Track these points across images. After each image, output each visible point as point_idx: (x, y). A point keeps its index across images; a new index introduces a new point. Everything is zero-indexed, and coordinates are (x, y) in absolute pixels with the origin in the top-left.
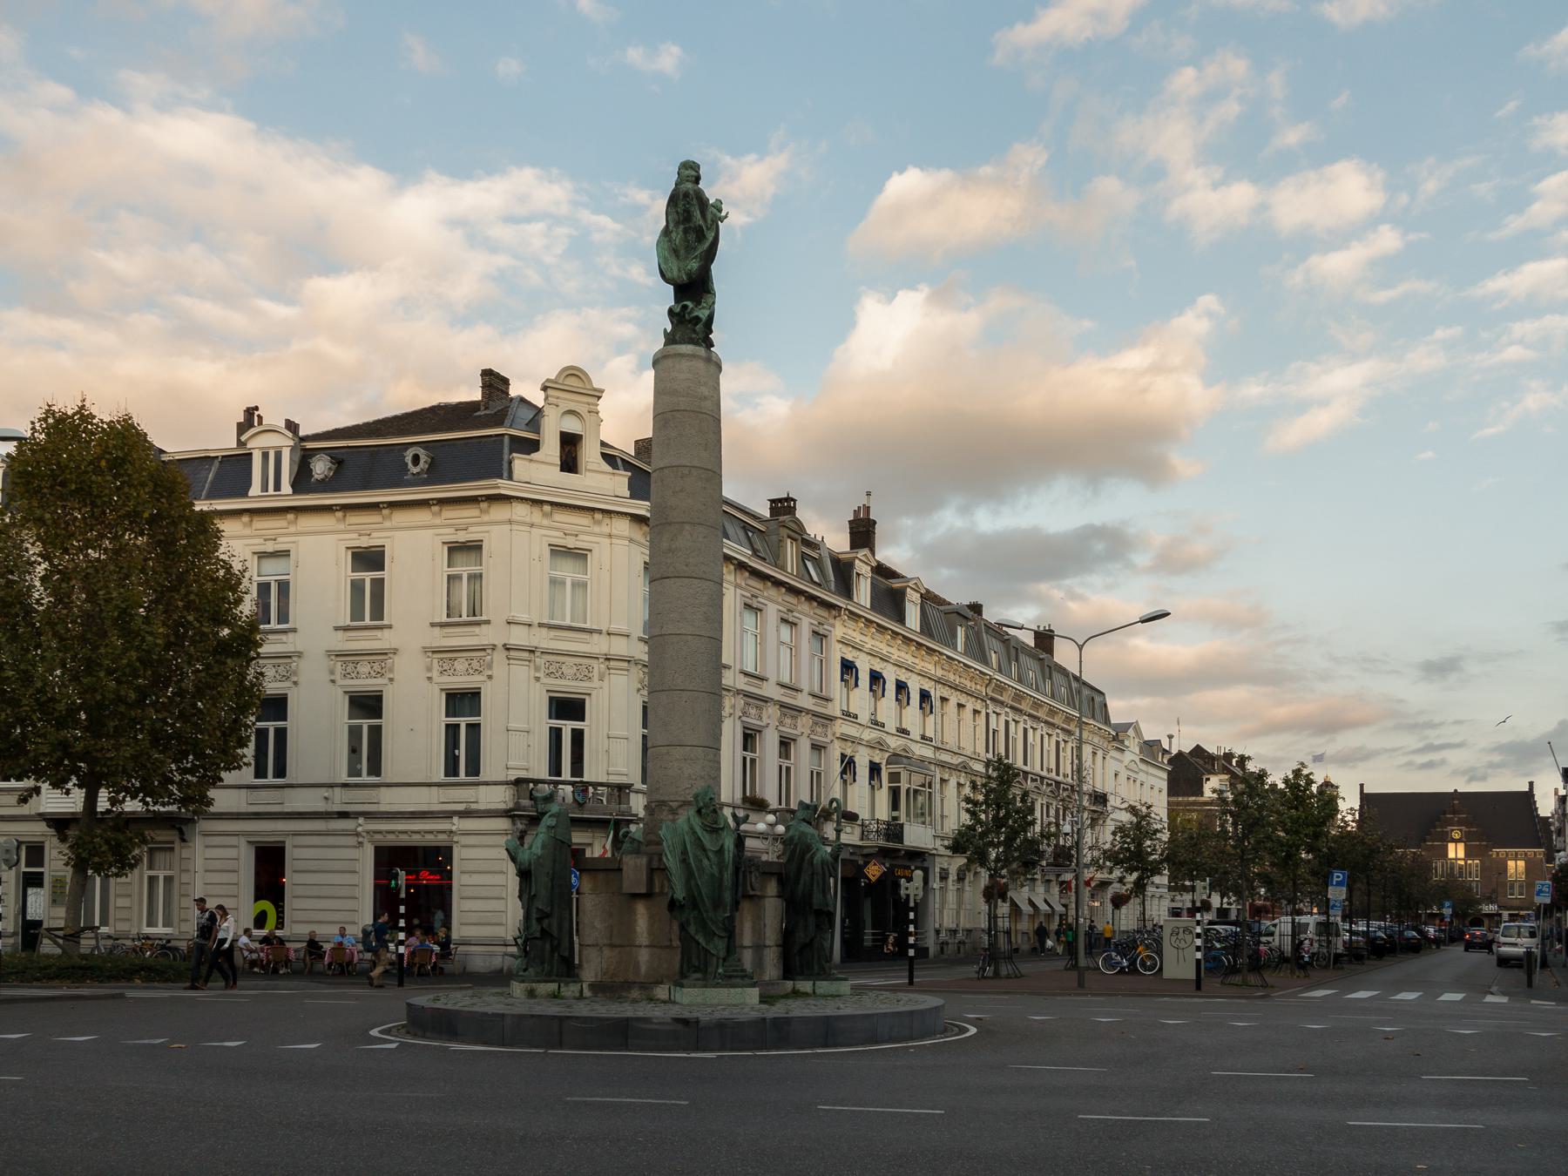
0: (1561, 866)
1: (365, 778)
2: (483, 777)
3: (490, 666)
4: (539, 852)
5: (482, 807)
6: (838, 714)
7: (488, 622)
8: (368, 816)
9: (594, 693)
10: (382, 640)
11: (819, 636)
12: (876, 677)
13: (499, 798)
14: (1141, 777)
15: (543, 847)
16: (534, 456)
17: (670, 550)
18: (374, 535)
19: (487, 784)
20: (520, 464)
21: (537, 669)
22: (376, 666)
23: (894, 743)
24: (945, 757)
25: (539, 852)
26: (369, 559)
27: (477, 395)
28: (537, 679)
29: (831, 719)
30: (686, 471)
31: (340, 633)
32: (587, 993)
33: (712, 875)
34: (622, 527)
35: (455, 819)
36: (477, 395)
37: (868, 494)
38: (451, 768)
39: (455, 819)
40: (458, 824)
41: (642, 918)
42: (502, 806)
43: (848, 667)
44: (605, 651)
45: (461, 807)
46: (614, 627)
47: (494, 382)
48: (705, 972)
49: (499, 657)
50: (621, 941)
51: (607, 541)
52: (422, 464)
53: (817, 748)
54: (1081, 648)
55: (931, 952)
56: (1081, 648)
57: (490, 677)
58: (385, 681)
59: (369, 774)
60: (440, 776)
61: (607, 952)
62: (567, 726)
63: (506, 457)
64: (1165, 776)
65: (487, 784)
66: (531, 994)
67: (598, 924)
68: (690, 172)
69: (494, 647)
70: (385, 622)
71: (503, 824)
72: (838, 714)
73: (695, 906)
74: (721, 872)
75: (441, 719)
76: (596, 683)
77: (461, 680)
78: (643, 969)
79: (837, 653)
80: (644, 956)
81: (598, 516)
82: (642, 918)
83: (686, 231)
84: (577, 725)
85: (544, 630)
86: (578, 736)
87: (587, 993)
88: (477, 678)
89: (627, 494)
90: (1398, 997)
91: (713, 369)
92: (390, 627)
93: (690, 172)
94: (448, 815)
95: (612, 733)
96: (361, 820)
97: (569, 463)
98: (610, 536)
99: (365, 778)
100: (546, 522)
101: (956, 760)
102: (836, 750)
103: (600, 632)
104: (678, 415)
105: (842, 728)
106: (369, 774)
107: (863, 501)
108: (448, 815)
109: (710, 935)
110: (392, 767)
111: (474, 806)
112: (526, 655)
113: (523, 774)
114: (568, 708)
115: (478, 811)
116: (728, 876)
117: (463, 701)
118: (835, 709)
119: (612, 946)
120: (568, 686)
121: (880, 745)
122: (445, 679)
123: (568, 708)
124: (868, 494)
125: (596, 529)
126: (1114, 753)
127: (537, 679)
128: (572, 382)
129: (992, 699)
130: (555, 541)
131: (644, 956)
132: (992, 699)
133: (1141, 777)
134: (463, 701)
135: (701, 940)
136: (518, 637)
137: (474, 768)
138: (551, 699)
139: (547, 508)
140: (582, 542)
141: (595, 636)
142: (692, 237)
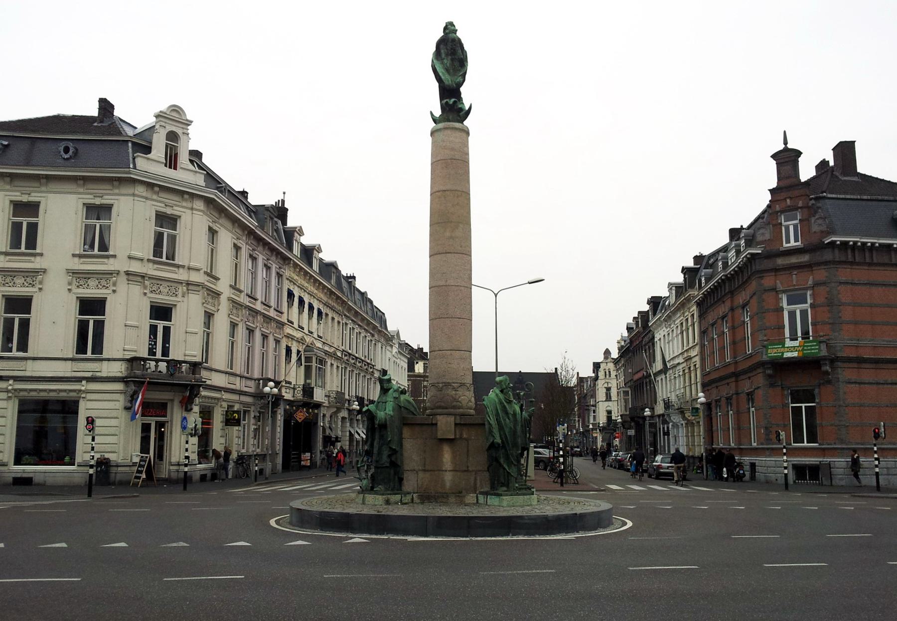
1: (15, 353)
2: (105, 355)
3: (114, 284)
5: (104, 374)
7: (114, 256)
8: (16, 379)
9: (179, 305)
10: (36, 263)
11: (279, 276)
12: (301, 301)
13: (118, 369)
14: (398, 361)
18: (33, 194)
20: (142, 163)
21: (145, 288)
22: (29, 280)
24: (327, 348)
26: (30, 209)
27: (94, 112)
29: (283, 324)
30: (459, 193)
31: (76, 259)
34: (199, 205)
35: (84, 382)
36: (94, 112)
38: (81, 347)
39: (84, 382)
40: (84, 386)
41: (447, 456)
42: (119, 375)
43: (291, 294)
44: (186, 279)
45: (89, 375)
46: (192, 264)
47: (106, 106)
48: (508, 486)
49: (123, 279)
50: (433, 468)
51: (189, 212)
52: (71, 152)
53: (277, 342)
58: (36, 289)
59: (18, 350)
60: (70, 352)
61: (421, 475)
63: (131, 155)
66: (388, 502)
67: (415, 457)
68: (449, 28)
69: (118, 273)
70: (38, 251)
71: (119, 386)
73: (504, 447)
74: (515, 427)
75: (146, 322)
76: (179, 298)
77: (92, 291)
78: (448, 485)
79: (286, 285)
80: (448, 477)
81: (186, 196)
82: (447, 456)
83: (452, 60)
84: (166, 323)
85: (151, 265)
86: (167, 330)
88: (104, 291)
91: (464, 135)
92: (41, 255)
93: (449, 28)
94: (79, 380)
95: (189, 330)
96: (11, 382)
97: (172, 161)
99: (15, 353)
100: (155, 197)
101: (332, 350)
102: (284, 343)
103: (183, 267)
105: (288, 330)
106: (18, 350)
107: (281, 197)
108: (79, 380)
110: (35, 346)
111: (98, 374)
112: (139, 279)
114: (161, 312)
115: (102, 378)
116: (519, 428)
117: (92, 307)
118: (284, 319)
119: (424, 471)
121: (301, 341)
122: (80, 290)
123: (161, 312)
125: (184, 204)
126: (388, 348)
127: (145, 294)
130: (14, 198)
131: (448, 477)
133: (398, 361)
134: (92, 307)
135: (506, 466)
136: (135, 267)
137: (98, 347)
138: (151, 306)
139: (157, 189)
140: (33, 198)
141: (181, 270)
142: (457, 64)
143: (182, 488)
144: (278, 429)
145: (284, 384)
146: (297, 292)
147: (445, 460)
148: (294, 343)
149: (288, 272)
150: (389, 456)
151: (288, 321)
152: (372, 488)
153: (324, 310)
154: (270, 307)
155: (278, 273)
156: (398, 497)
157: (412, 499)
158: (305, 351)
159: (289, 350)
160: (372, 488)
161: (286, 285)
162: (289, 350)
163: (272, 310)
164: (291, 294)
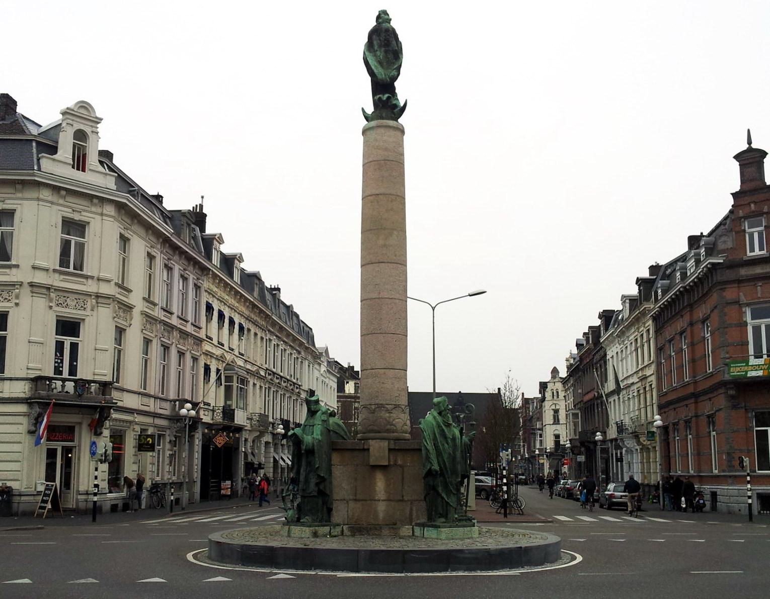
0: (522, 435)
3: (17, 297)
4: (319, 437)
6: (204, 338)
9: (87, 319)
11: (197, 287)
13: (21, 389)
15: (322, 434)
16: (54, 156)
17: (385, 245)
19: (11, 379)
20: (47, 164)
21: (51, 300)
23: (229, 357)
24: (249, 367)
25: (319, 437)
28: (51, 307)
30: (394, 197)
32: (346, 532)
33: (450, 454)
37: (202, 197)
43: (209, 308)
44: (95, 291)
46: (103, 275)
49: (26, 291)
50: (365, 497)
53: (195, 359)
54: (433, 309)
55: (240, 492)
56: (433, 309)
57: (17, 304)
61: (352, 504)
62: (68, 341)
63: (35, 156)
64: (336, 380)
65: (11, 379)
66: (315, 535)
69: (21, 284)
71: (23, 408)
72: (204, 338)
76: (88, 312)
79: (205, 298)
83: (386, 52)
84: (74, 339)
85: (57, 275)
86: (74, 347)
87: (346, 532)
89: (114, 187)
90: (555, 517)
91: (399, 133)
93: (383, 18)
95: (98, 346)
97: (80, 162)
98: (102, 214)
101: (254, 369)
102: (202, 361)
103: (92, 278)
104: (389, 163)
105: (207, 347)
107: (199, 202)
109: (449, 493)
112: (44, 291)
113: (38, 373)
114: (68, 327)
118: (202, 335)
119: (356, 500)
120: (71, 312)
121: (220, 359)
123: (68, 327)
124: (202, 197)
125: (93, 209)
127: (51, 307)
128: (82, 111)
129: (269, 331)
131: (381, 508)
132: (269, 331)
135: (444, 495)
141: (90, 281)
142: (391, 56)
144: (196, 455)
145: (202, 405)
146: (216, 306)
149: (206, 284)
150: (317, 484)
151: (207, 337)
152: (298, 520)
153: (246, 325)
155: (195, 285)
157: (342, 531)
159: (207, 369)
161: (205, 298)
162: (207, 369)
163: (189, 324)
164: (209, 308)
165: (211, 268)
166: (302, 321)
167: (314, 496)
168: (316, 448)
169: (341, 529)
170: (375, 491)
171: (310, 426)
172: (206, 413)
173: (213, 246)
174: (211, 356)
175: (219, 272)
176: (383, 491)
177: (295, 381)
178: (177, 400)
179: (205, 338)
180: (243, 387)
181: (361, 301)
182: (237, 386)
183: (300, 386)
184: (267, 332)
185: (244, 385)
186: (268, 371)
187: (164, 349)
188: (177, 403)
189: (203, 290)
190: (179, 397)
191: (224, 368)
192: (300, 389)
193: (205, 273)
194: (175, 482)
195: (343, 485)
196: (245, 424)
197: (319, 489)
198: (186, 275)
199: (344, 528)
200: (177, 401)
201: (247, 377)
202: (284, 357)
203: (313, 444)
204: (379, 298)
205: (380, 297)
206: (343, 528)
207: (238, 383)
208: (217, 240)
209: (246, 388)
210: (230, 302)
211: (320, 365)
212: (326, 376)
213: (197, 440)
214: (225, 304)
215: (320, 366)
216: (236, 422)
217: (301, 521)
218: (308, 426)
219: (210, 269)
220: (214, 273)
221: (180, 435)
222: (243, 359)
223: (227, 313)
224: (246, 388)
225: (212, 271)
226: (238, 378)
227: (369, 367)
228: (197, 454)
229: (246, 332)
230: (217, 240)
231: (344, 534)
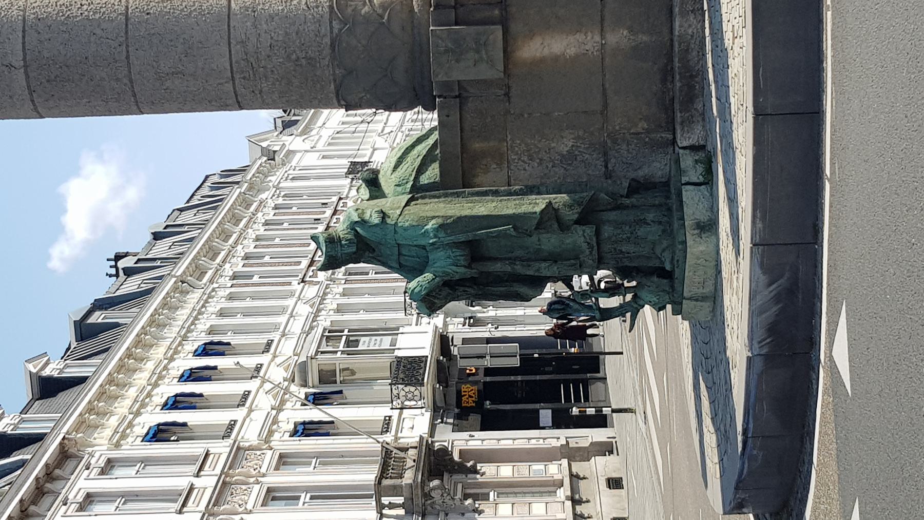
6: (230, 441)
43: (159, 434)
53: (284, 460)
79: (135, 447)
118: (221, 449)
129: (211, 281)
143: (600, 384)
144: (506, 444)
145: (389, 438)
146: (154, 417)
147: (572, 51)
148: (282, 416)
149: (100, 446)
150: (563, 227)
151: (226, 436)
152: (667, 275)
153: (199, 338)
154: (191, 489)
155: (103, 472)
156: (688, 194)
157: (693, 148)
158: (305, 385)
159: (306, 429)
160: (667, 275)
161: (135, 447)
162: (306, 429)
163: (198, 482)
164: (159, 434)
165: (61, 436)
166: (188, 202)
167: (598, 233)
168: (462, 238)
169: (687, 152)
170: (577, 56)
171: (400, 254)
172: (407, 424)
173: (9, 432)
174: (274, 423)
175: (68, 419)
176: (577, 36)
177: (329, 212)
178: (378, 501)
179: (230, 441)
180: (344, 338)
181: (42, 117)
182: (343, 352)
183: (340, 199)
184: (215, 285)
185: (342, 336)
186: (307, 279)
187: (274, 499)
188: (385, 500)
189: (115, 454)
190: (370, 497)
191: (302, 386)
192: (347, 197)
193: (73, 450)
194: (569, 493)
195: (564, 149)
196: (430, 329)
197: (578, 222)
198: (80, 498)
199: (685, 144)
200: (380, 500)
201: (320, 330)
202: (251, 277)
203: (457, 245)
204: (26, 66)
205: (22, 63)
206: (684, 148)
207: (336, 352)
208: (43, 368)
209: (346, 332)
210: (145, 382)
211: (291, 153)
212: (317, 137)
213: (470, 443)
214: (166, 368)
215: (294, 152)
216: (426, 352)
217: (668, 267)
218: (402, 258)
219: (64, 438)
220: (78, 426)
221: (460, 486)
222: (279, 341)
223: (171, 388)
224: (346, 332)
225: (67, 433)
226: (322, 352)
227: (229, 87)
228: (502, 442)
229: (216, 339)
230: (43, 368)
231: (702, 143)
